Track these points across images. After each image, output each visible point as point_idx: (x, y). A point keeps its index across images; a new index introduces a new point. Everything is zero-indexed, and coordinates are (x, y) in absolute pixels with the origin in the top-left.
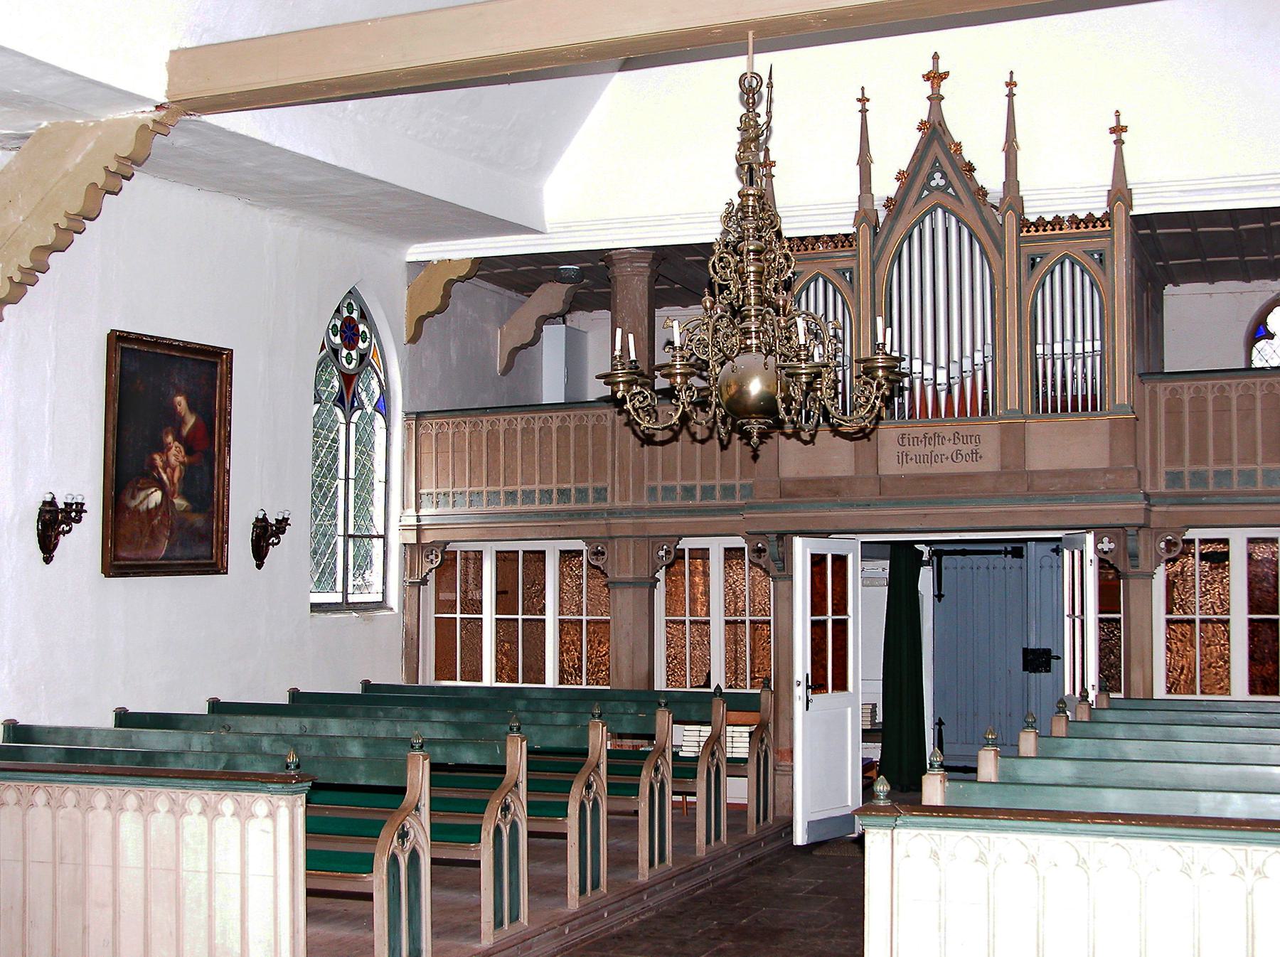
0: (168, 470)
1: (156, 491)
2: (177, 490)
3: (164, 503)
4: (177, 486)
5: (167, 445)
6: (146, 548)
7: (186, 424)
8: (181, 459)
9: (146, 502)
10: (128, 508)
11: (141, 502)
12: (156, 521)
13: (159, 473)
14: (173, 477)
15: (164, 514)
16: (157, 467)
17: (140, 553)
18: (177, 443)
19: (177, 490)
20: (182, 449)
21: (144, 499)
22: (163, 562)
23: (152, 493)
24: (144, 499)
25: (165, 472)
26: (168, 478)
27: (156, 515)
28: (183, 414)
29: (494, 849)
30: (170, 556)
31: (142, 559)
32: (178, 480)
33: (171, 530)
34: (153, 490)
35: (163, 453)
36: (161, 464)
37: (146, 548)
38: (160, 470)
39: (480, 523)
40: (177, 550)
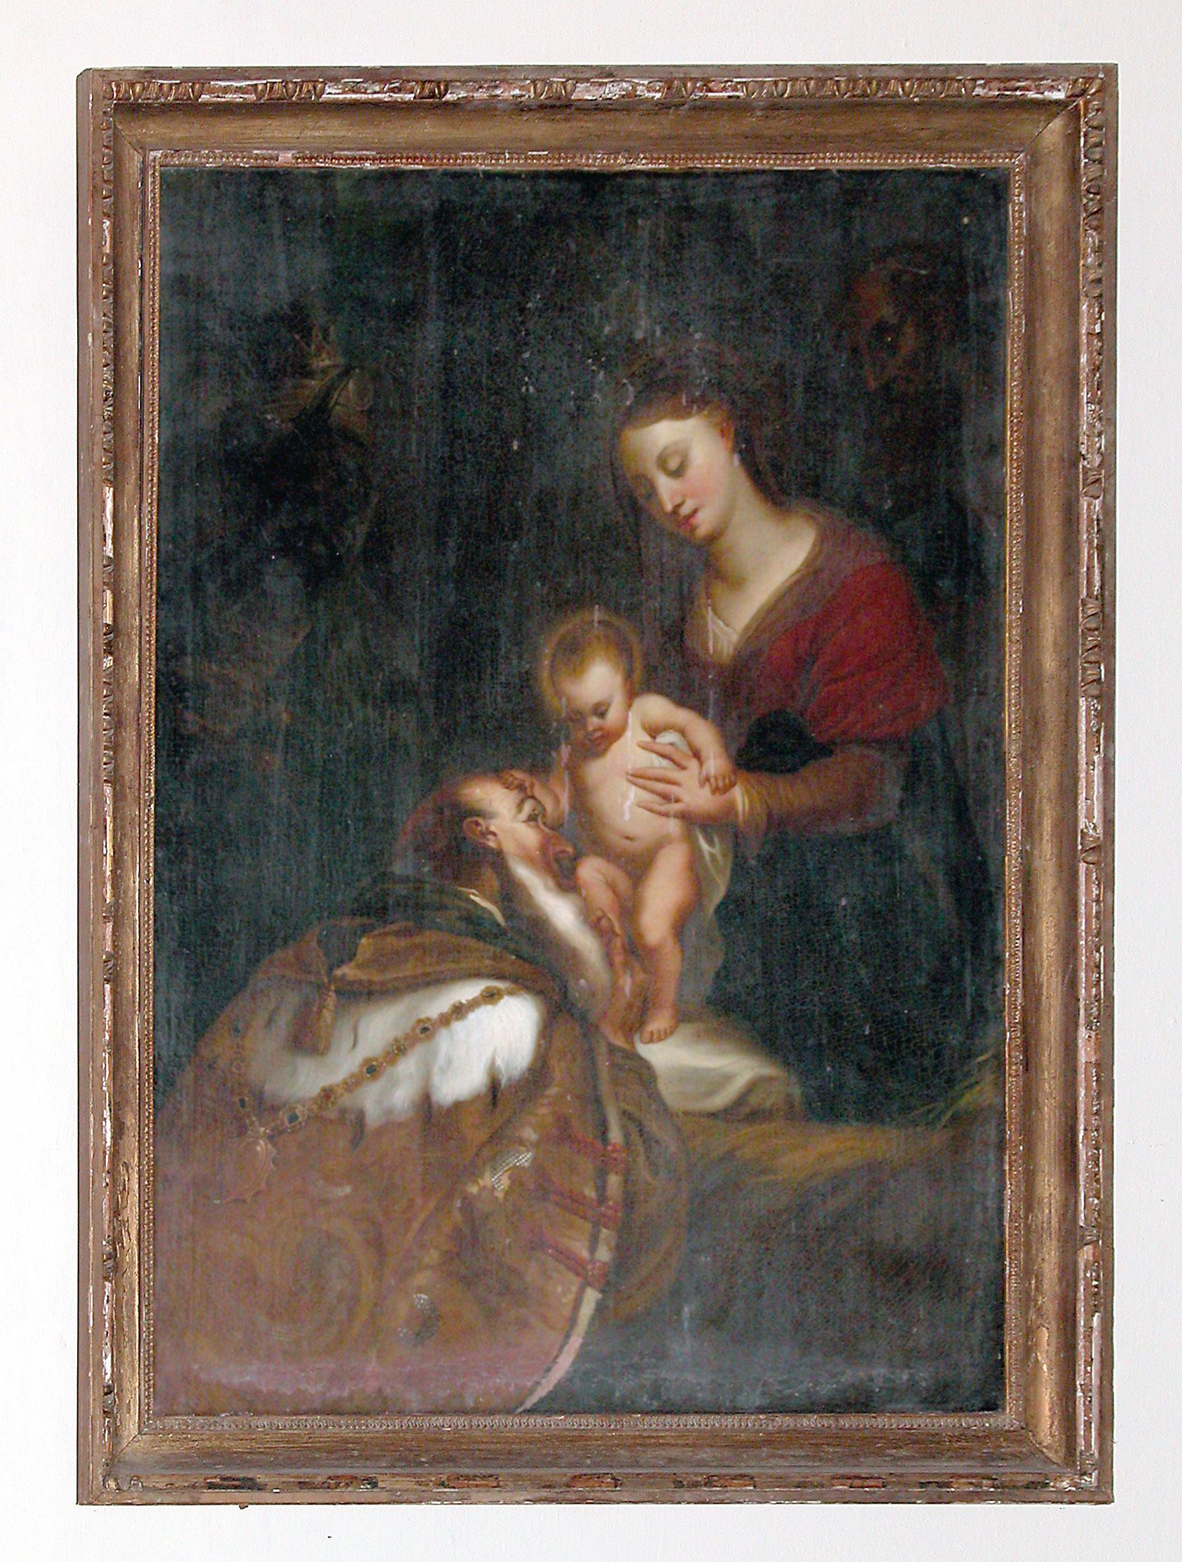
0: (591, 870)
1: (491, 997)
2: (669, 992)
3: (558, 1069)
4: (671, 962)
5: (578, 717)
6: (833, 1196)
7: (736, 583)
8: (698, 798)
9: (408, 1067)
10: (266, 1107)
11: (372, 1070)
12: (496, 1181)
13: (511, 893)
14: (630, 910)
15: (562, 1132)
16: (498, 860)
17: (372, 1366)
18: (656, 707)
19: (669, 992)
20: (704, 734)
21: (398, 1050)
22: (559, 1421)
23: (459, 1011)
24: (398, 1050)
25: (566, 881)
26: (594, 922)
27: (499, 1140)
28: (705, 522)
29: (1077, 736)
30: (622, 1387)
31: (383, 1406)
32: (679, 928)
33: (624, 1229)
34: (468, 991)
35: (541, 768)
36: (530, 836)
37: (833, 1196)
38: (524, 873)
39: (134, 967)
40: (682, 1347)
